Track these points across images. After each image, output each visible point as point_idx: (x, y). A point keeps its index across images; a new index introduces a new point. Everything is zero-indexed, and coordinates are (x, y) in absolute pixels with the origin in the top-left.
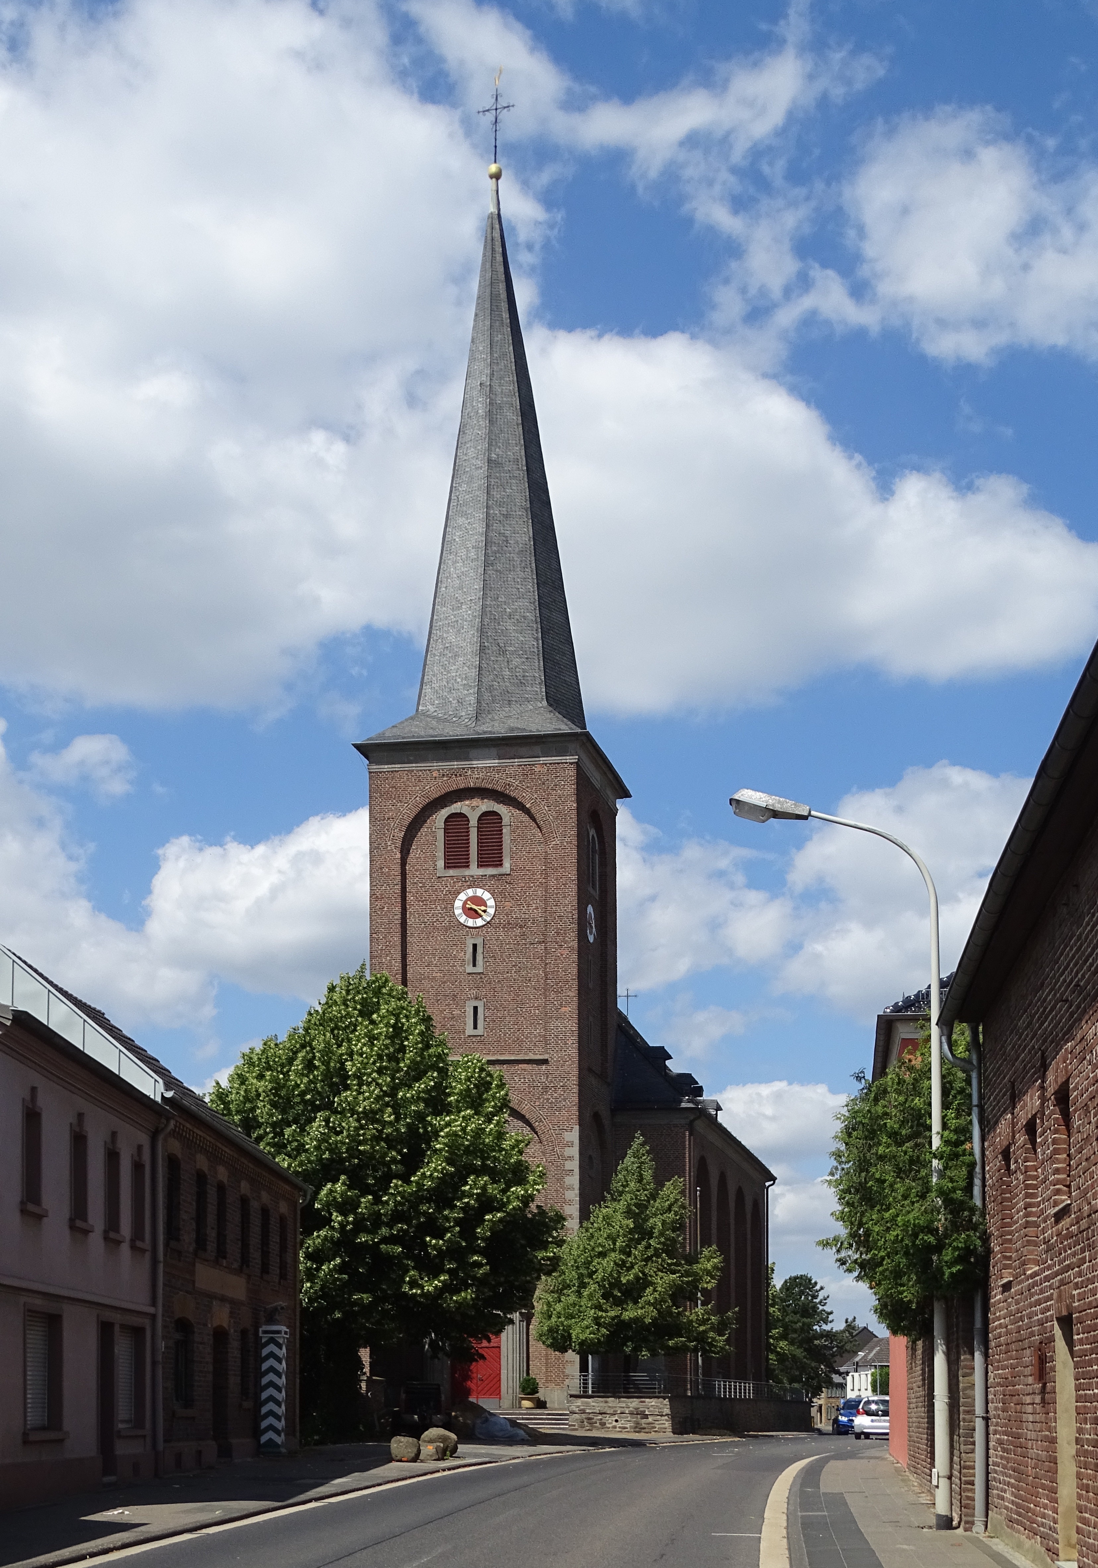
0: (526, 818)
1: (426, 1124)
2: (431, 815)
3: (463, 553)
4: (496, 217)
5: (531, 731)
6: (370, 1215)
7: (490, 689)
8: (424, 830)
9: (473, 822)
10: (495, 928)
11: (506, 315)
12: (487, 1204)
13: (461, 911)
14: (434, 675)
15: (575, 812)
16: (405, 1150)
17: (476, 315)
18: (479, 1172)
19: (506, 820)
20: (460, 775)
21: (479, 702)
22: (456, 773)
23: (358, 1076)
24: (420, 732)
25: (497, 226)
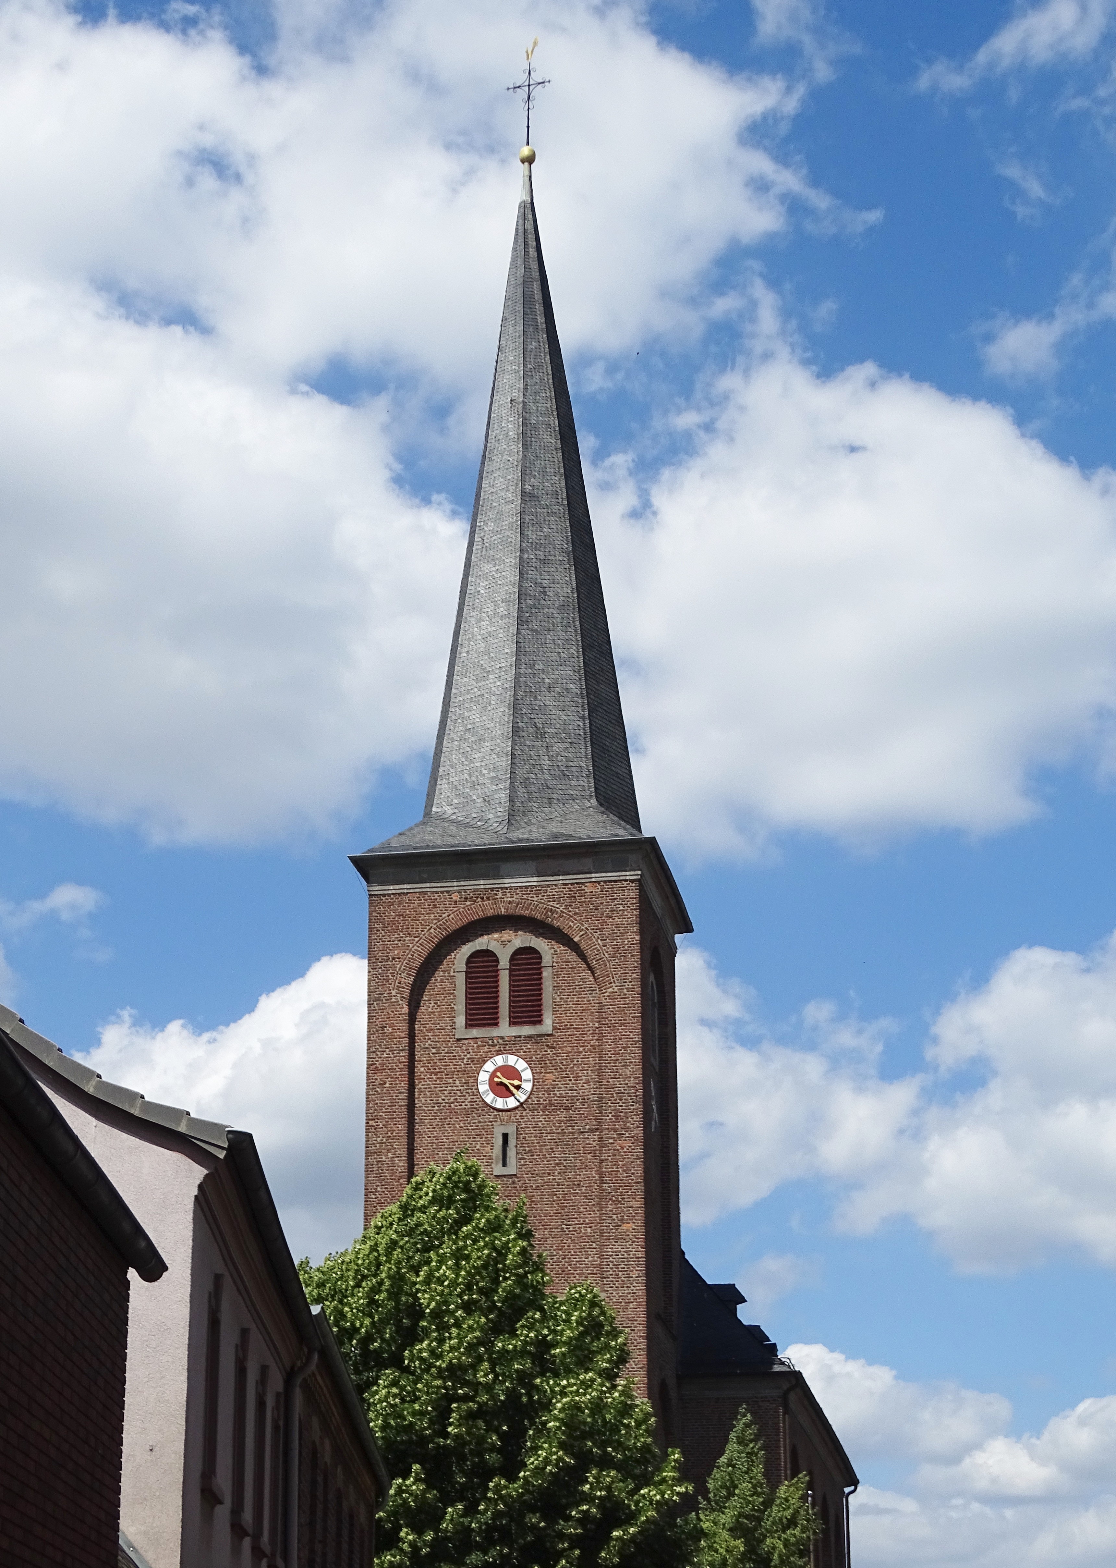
0: (573, 957)
1: (532, 1388)
2: (449, 954)
3: (490, 608)
4: (529, 206)
5: (580, 838)
6: (456, 1532)
7: (526, 782)
8: (439, 974)
9: (504, 962)
10: (533, 1110)
11: (541, 319)
12: (614, 1513)
13: (487, 1087)
14: (452, 766)
15: (637, 947)
16: (505, 1428)
17: (504, 319)
18: (605, 1463)
19: (547, 960)
20: (488, 898)
21: (511, 800)
22: (483, 895)
23: (437, 1314)
24: (434, 839)
25: (530, 217)
